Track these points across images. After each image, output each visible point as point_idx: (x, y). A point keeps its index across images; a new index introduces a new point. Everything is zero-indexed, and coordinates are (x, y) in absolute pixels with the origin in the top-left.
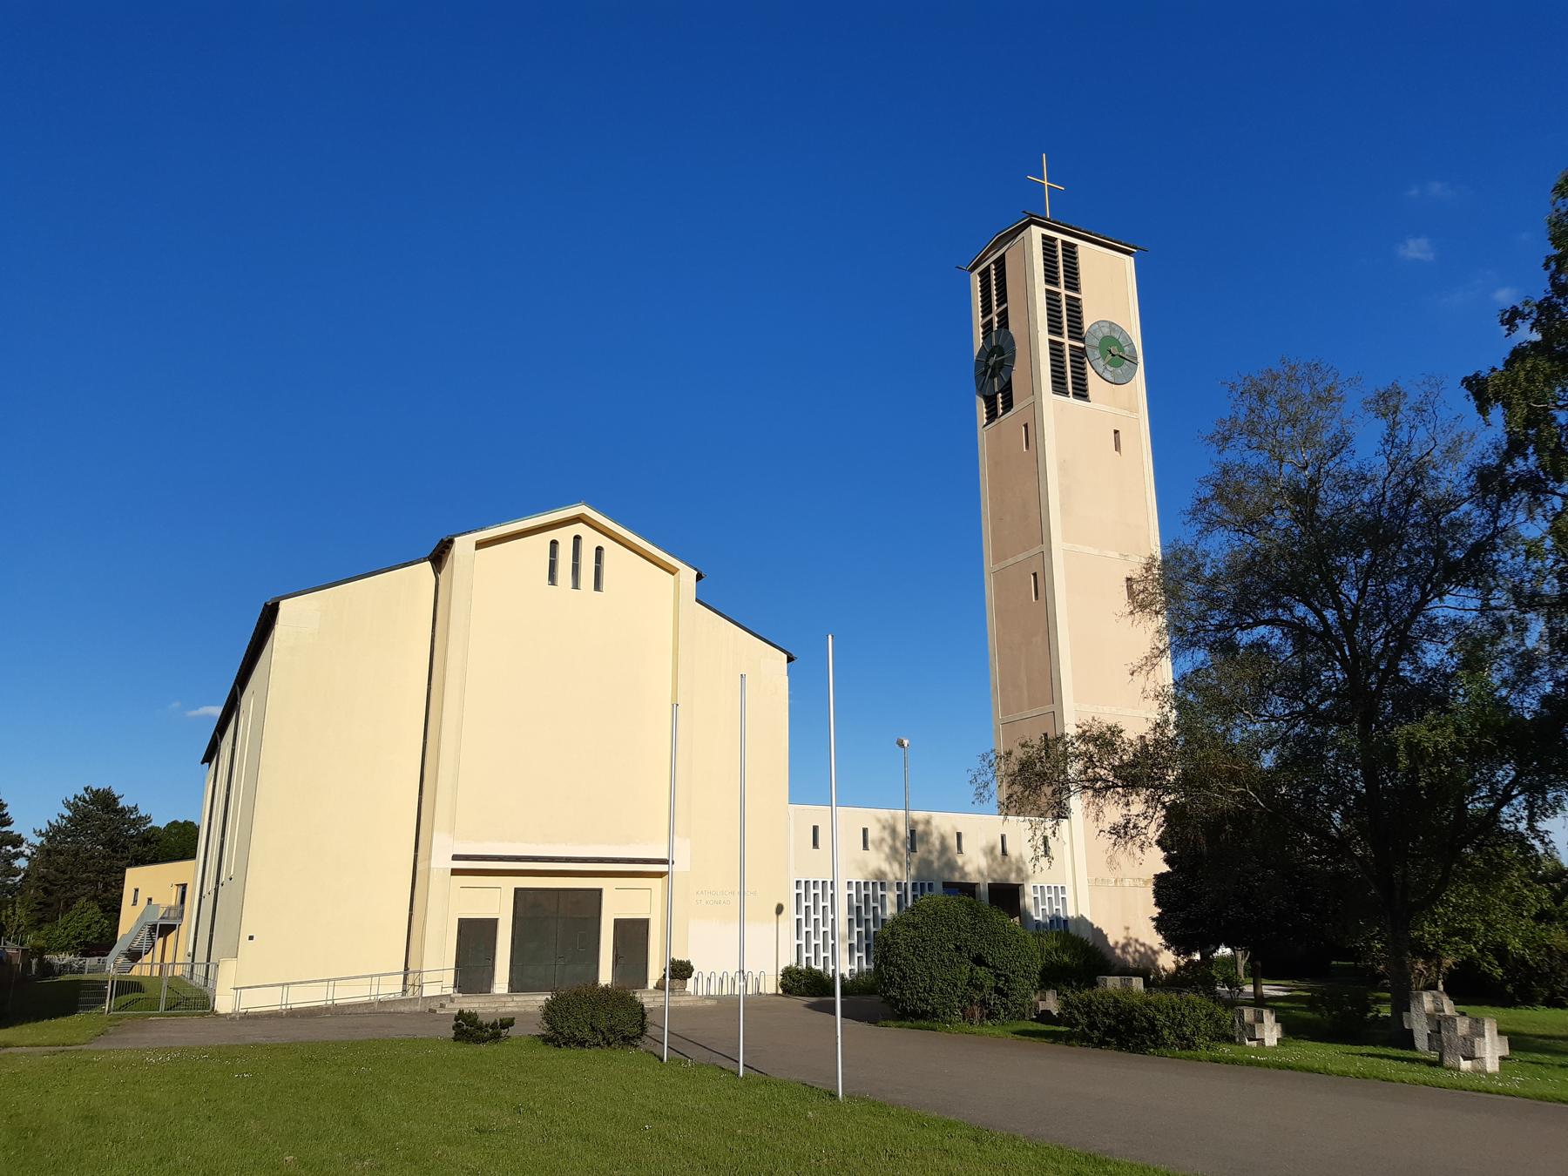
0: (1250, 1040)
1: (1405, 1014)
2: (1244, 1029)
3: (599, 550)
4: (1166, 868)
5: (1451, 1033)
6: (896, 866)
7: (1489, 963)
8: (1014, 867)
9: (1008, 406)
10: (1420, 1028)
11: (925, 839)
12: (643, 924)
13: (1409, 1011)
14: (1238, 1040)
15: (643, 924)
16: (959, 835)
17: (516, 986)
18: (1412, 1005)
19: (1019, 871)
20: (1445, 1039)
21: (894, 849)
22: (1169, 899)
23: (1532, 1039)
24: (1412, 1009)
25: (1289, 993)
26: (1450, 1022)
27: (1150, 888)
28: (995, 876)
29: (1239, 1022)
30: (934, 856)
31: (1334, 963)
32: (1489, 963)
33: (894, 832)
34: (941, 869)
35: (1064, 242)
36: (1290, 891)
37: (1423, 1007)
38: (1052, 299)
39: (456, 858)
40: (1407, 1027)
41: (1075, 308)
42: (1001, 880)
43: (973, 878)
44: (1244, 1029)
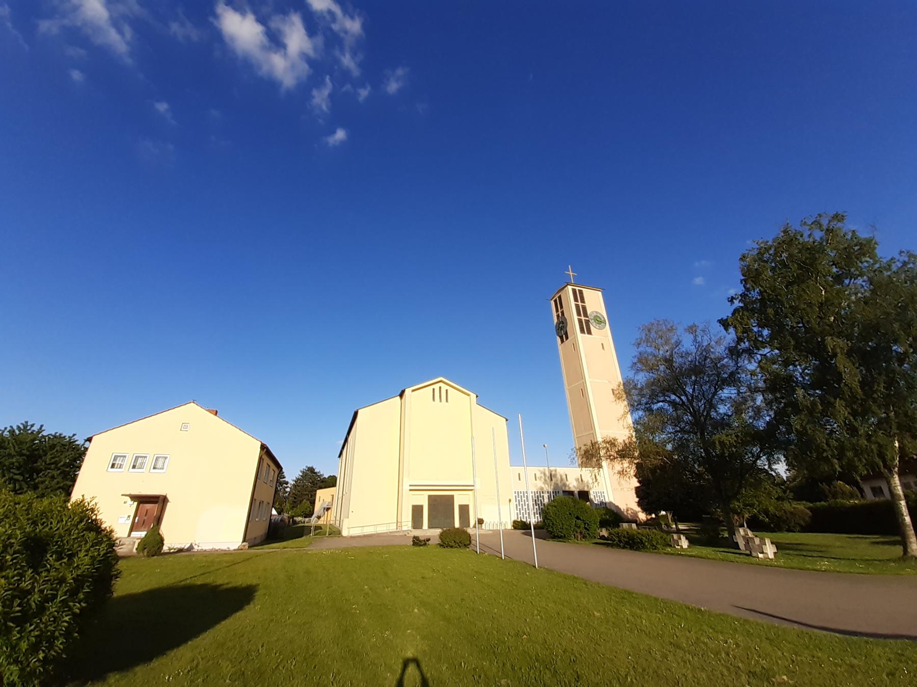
3: (447, 390)
9: (567, 338)
12: (467, 506)
15: (467, 506)
17: (429, 527)
30: (559, 482)
33: (545, 474)
35: (579, 290)
38: (577, 306)
39: (410, 486)
41: (584, 308)
43: (572, 489)
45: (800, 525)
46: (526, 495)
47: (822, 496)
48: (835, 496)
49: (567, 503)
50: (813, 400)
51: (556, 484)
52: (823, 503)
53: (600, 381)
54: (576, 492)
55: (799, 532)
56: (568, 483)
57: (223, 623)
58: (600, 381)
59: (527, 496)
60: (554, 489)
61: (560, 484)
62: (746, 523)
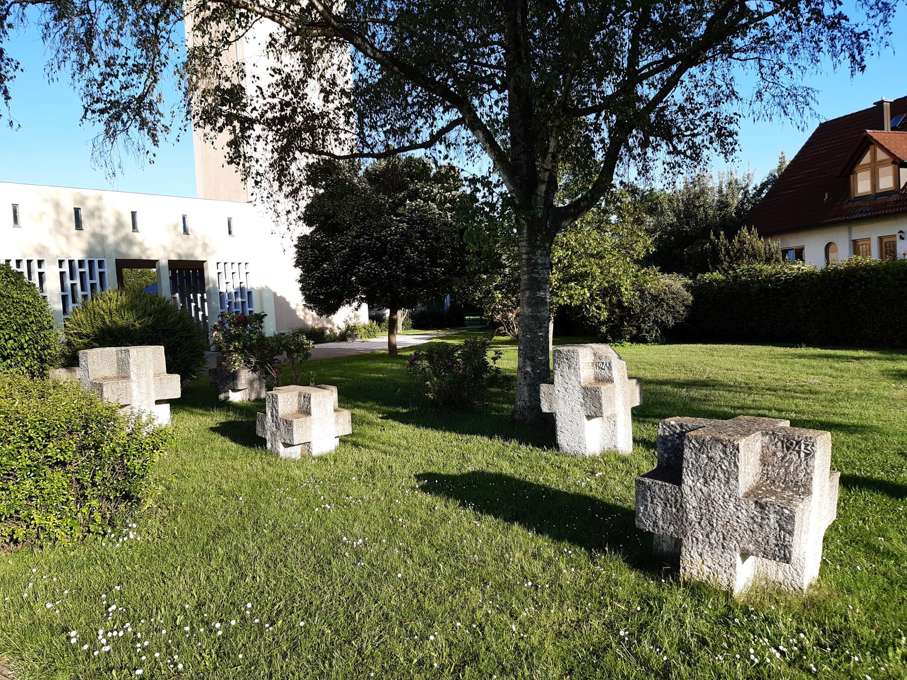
0: (286, 445)
1: (544, 387)
2: (278, 428)
4: (307, 230)
5: (714, 485)
6: (62, 240)
7: (599, 308)
8: (200, 243)
10: (569, 411)
11: (97, 214)
13: (552, 382)
14: (269, 445)
16: (134, 214)
18: (558, 372)
19: (205, 246)
20: (692, 502)
21: (59, 223)
22: (306, 259)
23: (668, 388)
24: (557, 379)
25: (429, 341)
26: (717, 454)
27: (292, 253)
28: (179, 251)
29: (272, 416)
30: (109, 232)
31: (467, 317)
32: (599, 308)
33: (57, 206)
34: (117, 244)
36: (422, 246)
37: (578, 376)
40: (545, 409)
42: (186, 255)
43: (154, 254)
44: (278, 428)
45: (663, 326)
46: (97, 270)
47: (711, 260)
48: (737, 257)
49: (791, 108)
50: (408, 187)
51: (100, 238)
52: (717, 275)
53: (335, 378)
54: (164, 262)
55: (656, 341)
56: (138, 237)
57: (108, 348)
58: (335, 378)
59: (101, 274)
60: (90, 251)
61: (111, 239)
62: (554, 323)
